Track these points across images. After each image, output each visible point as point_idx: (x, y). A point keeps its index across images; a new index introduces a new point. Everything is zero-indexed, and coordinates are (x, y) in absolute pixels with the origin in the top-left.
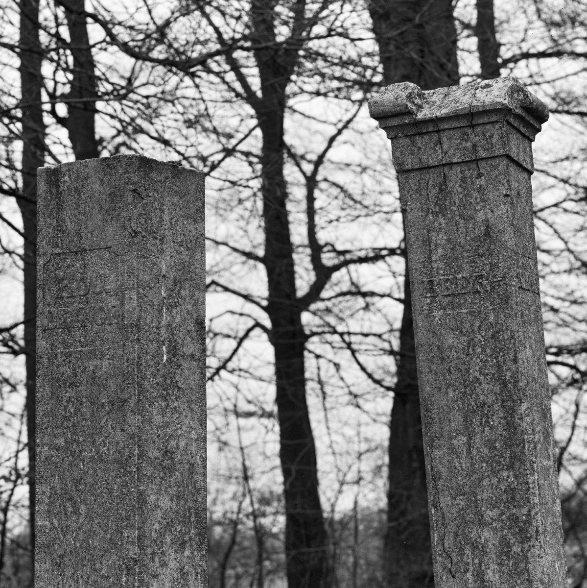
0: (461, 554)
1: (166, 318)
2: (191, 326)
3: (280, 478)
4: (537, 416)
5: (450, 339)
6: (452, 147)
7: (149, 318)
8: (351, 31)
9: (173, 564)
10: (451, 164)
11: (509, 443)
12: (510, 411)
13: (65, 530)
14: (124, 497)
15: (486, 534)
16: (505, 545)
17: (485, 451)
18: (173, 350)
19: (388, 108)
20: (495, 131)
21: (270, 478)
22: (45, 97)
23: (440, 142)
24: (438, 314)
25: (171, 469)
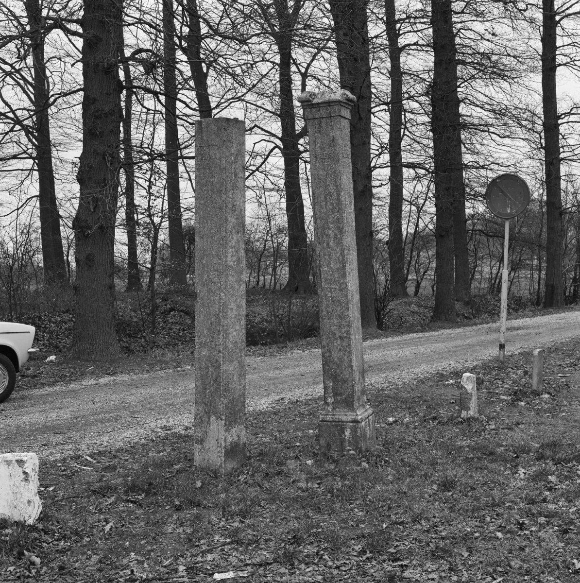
0: (323, 237)
1: (233, 166)
2: (241, 168)
3: (286, 218)
4: (347, 197)
5: (321, 173)
6: (323, 112)
7: (229, 166)
8: (318, 13)
9: (235, 238)
10: (323, 118)
11: (338, 205)
12: (339, 195)
13: (204, 228)
14: (221, 218)
15: (330, 232)
16: (336, 236)
17: (331, 207)
18: (236, 176)
19: (304, 99)
20: (336, 108)
21: (282, 219)
22: (176, 39)
23: (319, 111)
24: (318, 164)
25: (235, 211)
